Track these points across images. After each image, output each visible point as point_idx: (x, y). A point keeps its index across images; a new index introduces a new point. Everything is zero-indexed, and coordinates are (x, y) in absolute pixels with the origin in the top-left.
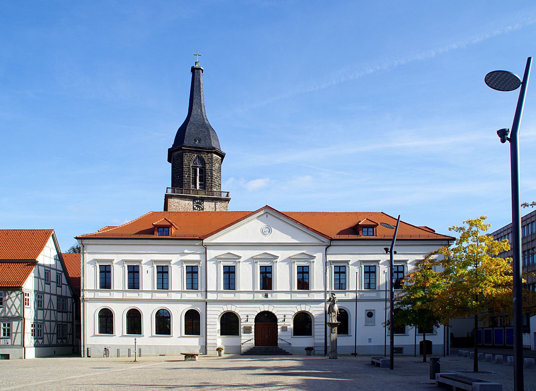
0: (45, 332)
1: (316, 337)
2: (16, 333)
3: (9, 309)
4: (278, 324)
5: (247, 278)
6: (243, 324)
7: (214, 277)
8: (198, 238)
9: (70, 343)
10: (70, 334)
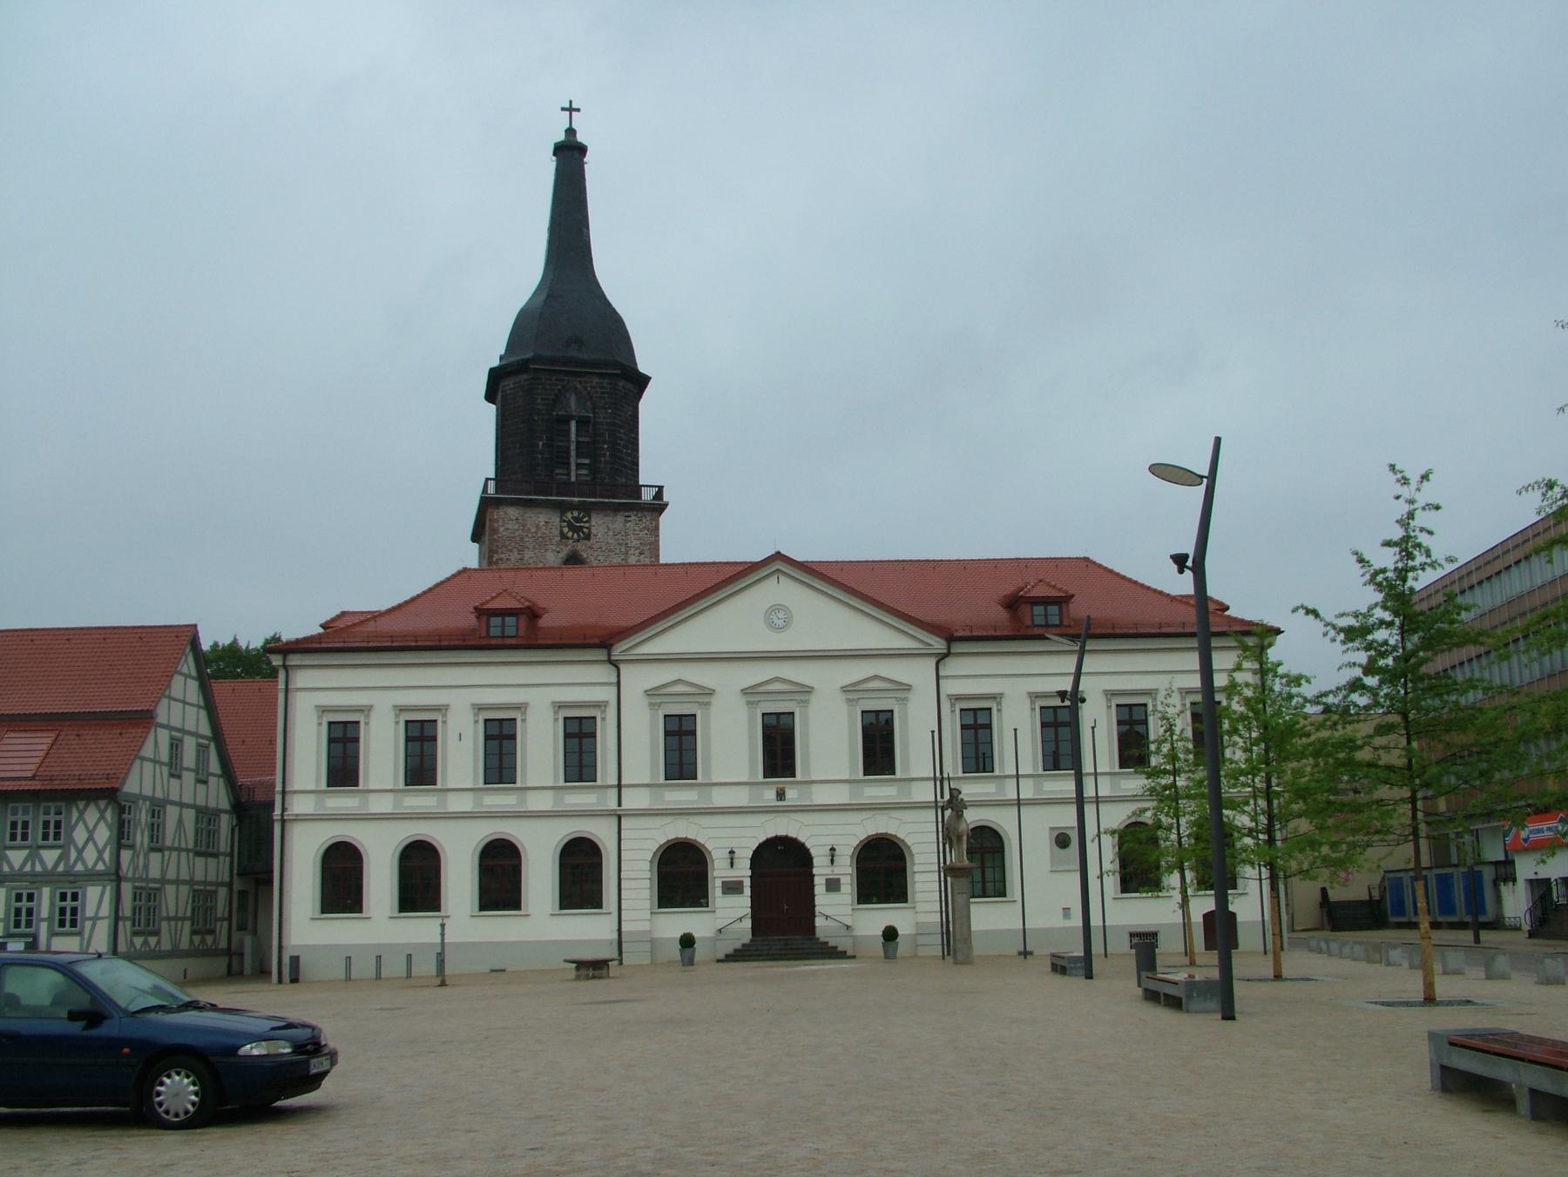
0: (164, 914)
1: (919, 907)
2: (95, 919)
3: (80, 852)
4: (815, 871)
5: (729, 746)
6: (719, 872)
7: (636, 747)
8: (596, 641)
9: (223, 944)
10: (223, 919)
